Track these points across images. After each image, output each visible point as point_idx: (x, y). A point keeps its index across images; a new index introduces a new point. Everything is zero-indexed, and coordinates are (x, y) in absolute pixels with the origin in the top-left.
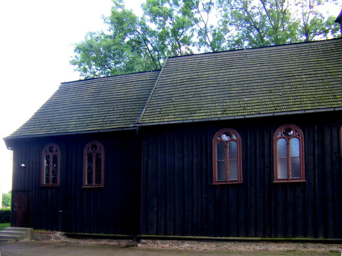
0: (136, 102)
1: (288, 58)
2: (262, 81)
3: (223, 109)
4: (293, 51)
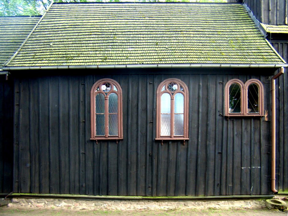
0: (12, 46)
1: (177, 15)
2: (148, 33)
3: (104, 57)
4: (183, 9)
